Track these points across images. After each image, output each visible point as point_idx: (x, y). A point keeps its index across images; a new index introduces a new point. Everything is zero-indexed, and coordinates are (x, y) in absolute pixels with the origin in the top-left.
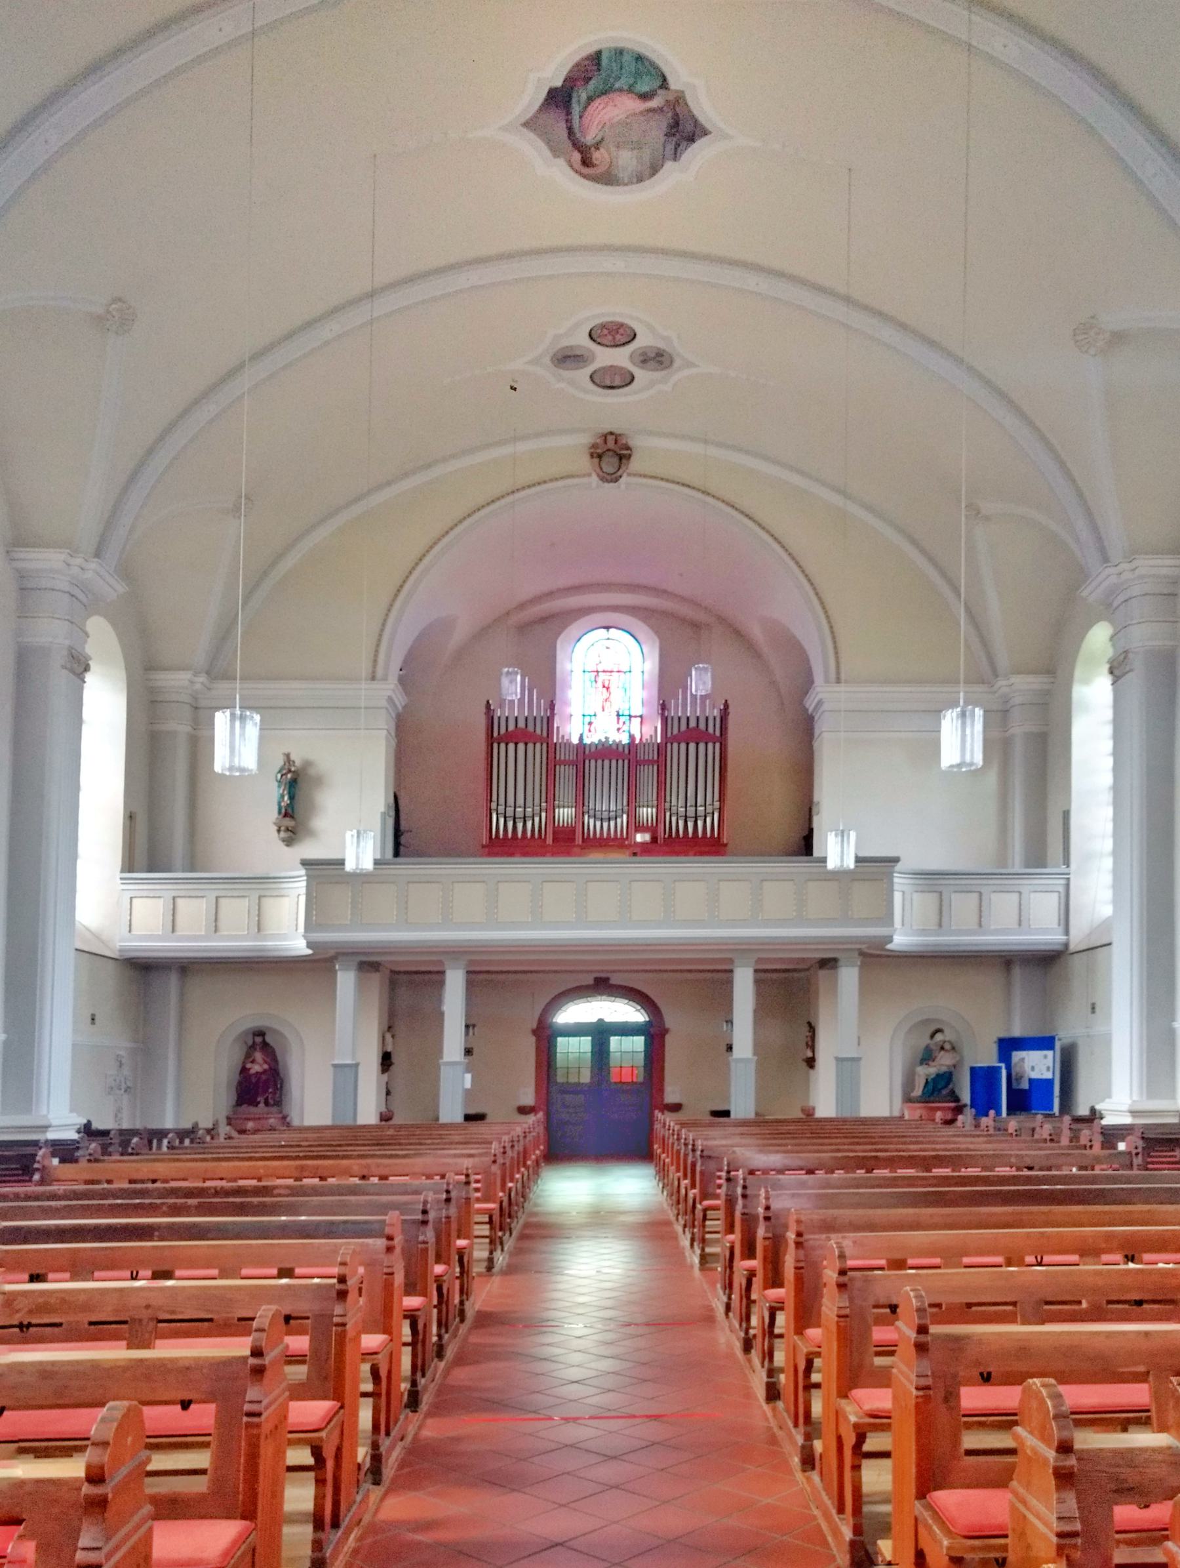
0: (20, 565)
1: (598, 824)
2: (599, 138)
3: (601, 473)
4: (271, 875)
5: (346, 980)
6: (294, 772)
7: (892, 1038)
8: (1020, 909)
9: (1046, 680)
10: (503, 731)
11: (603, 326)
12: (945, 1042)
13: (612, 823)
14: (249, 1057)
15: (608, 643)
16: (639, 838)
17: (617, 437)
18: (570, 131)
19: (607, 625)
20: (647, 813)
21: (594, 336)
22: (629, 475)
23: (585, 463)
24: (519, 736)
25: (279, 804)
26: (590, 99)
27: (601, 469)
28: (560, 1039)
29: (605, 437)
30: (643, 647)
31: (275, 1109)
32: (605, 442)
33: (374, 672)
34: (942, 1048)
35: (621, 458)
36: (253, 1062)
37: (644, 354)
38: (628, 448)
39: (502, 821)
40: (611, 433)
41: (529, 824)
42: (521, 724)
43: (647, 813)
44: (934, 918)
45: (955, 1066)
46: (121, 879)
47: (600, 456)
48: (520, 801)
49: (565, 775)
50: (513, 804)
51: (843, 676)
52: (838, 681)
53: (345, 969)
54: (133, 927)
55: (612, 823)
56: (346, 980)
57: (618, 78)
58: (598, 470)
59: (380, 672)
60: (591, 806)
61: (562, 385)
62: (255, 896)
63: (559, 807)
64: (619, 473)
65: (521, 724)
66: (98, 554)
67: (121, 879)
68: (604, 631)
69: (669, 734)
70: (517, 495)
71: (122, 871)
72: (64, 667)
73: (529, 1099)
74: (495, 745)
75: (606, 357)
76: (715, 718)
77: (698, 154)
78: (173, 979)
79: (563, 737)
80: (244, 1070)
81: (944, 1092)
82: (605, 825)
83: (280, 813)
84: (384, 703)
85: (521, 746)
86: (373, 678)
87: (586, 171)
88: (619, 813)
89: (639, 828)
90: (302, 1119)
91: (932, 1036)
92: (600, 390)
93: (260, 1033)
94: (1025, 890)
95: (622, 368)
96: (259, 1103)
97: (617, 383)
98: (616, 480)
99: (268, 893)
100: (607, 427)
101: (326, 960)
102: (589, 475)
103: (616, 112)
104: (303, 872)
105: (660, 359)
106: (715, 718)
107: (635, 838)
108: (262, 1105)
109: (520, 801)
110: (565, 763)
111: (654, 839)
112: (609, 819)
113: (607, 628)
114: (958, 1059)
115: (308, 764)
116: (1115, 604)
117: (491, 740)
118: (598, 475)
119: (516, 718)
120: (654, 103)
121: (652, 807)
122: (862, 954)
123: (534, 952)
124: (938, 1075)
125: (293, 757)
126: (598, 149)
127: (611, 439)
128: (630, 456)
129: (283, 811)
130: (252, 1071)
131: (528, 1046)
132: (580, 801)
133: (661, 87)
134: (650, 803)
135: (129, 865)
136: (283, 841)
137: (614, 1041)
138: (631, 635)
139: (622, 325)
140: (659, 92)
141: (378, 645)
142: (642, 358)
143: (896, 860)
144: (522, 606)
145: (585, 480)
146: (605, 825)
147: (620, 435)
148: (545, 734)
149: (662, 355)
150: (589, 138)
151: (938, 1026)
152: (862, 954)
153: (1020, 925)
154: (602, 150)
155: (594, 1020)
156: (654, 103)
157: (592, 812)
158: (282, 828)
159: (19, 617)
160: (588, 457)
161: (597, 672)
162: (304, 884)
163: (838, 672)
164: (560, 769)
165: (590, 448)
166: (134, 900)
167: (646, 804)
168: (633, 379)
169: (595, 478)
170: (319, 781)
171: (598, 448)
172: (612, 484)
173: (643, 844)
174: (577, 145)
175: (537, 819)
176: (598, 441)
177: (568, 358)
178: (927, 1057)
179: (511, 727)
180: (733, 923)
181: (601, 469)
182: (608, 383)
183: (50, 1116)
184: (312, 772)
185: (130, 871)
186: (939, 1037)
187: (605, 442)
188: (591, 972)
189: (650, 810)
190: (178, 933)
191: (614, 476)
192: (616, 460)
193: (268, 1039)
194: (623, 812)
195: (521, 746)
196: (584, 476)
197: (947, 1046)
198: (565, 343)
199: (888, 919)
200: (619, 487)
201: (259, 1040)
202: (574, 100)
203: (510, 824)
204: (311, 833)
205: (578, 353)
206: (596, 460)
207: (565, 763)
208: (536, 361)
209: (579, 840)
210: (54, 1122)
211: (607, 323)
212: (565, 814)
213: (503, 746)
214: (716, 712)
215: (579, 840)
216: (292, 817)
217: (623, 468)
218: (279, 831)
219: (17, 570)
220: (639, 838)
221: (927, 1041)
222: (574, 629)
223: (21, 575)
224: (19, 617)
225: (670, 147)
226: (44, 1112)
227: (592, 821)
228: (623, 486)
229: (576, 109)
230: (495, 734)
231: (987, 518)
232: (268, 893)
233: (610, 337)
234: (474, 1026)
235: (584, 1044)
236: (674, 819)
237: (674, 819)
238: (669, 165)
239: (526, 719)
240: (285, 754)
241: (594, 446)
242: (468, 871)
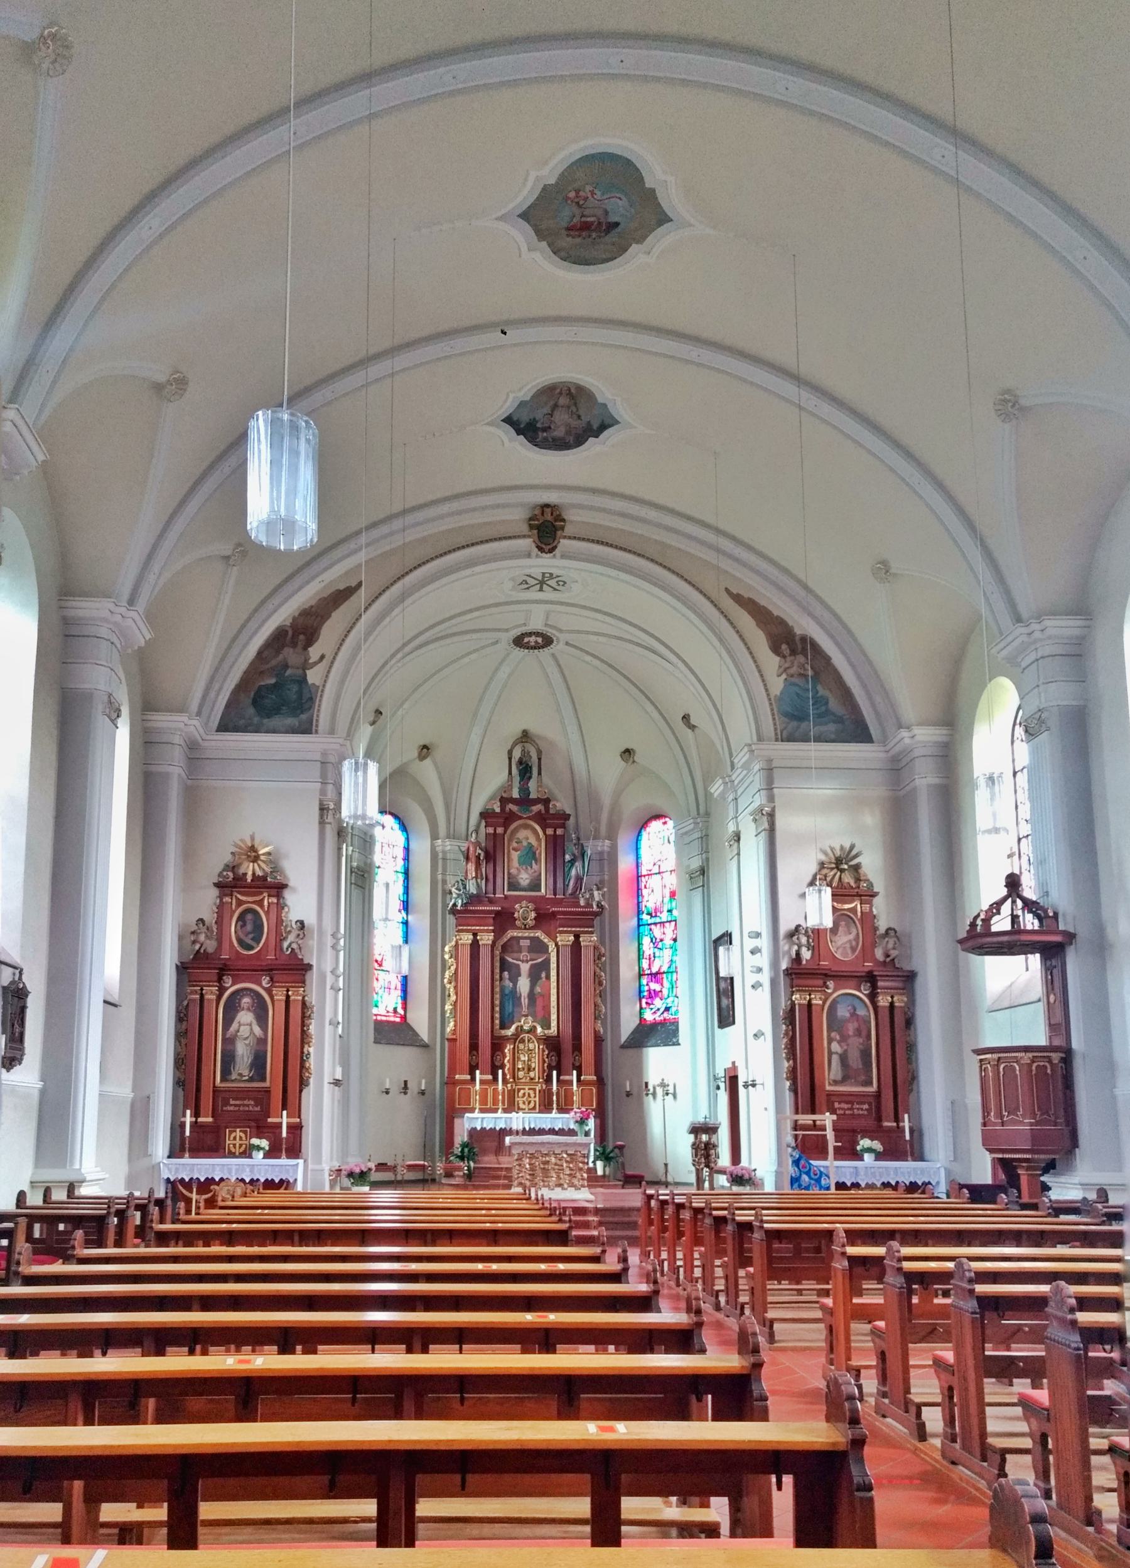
0: (149, 724)
9: (945, 732)
32: (543, 514)
38: (564, 520)
116: (1024, 665)
127: (548, 510)
165: (530, 519)
183: (83, 1171)
187: (543, 514)
188: (324, 686)
210: (88, 1179)
226: (77, 1167)
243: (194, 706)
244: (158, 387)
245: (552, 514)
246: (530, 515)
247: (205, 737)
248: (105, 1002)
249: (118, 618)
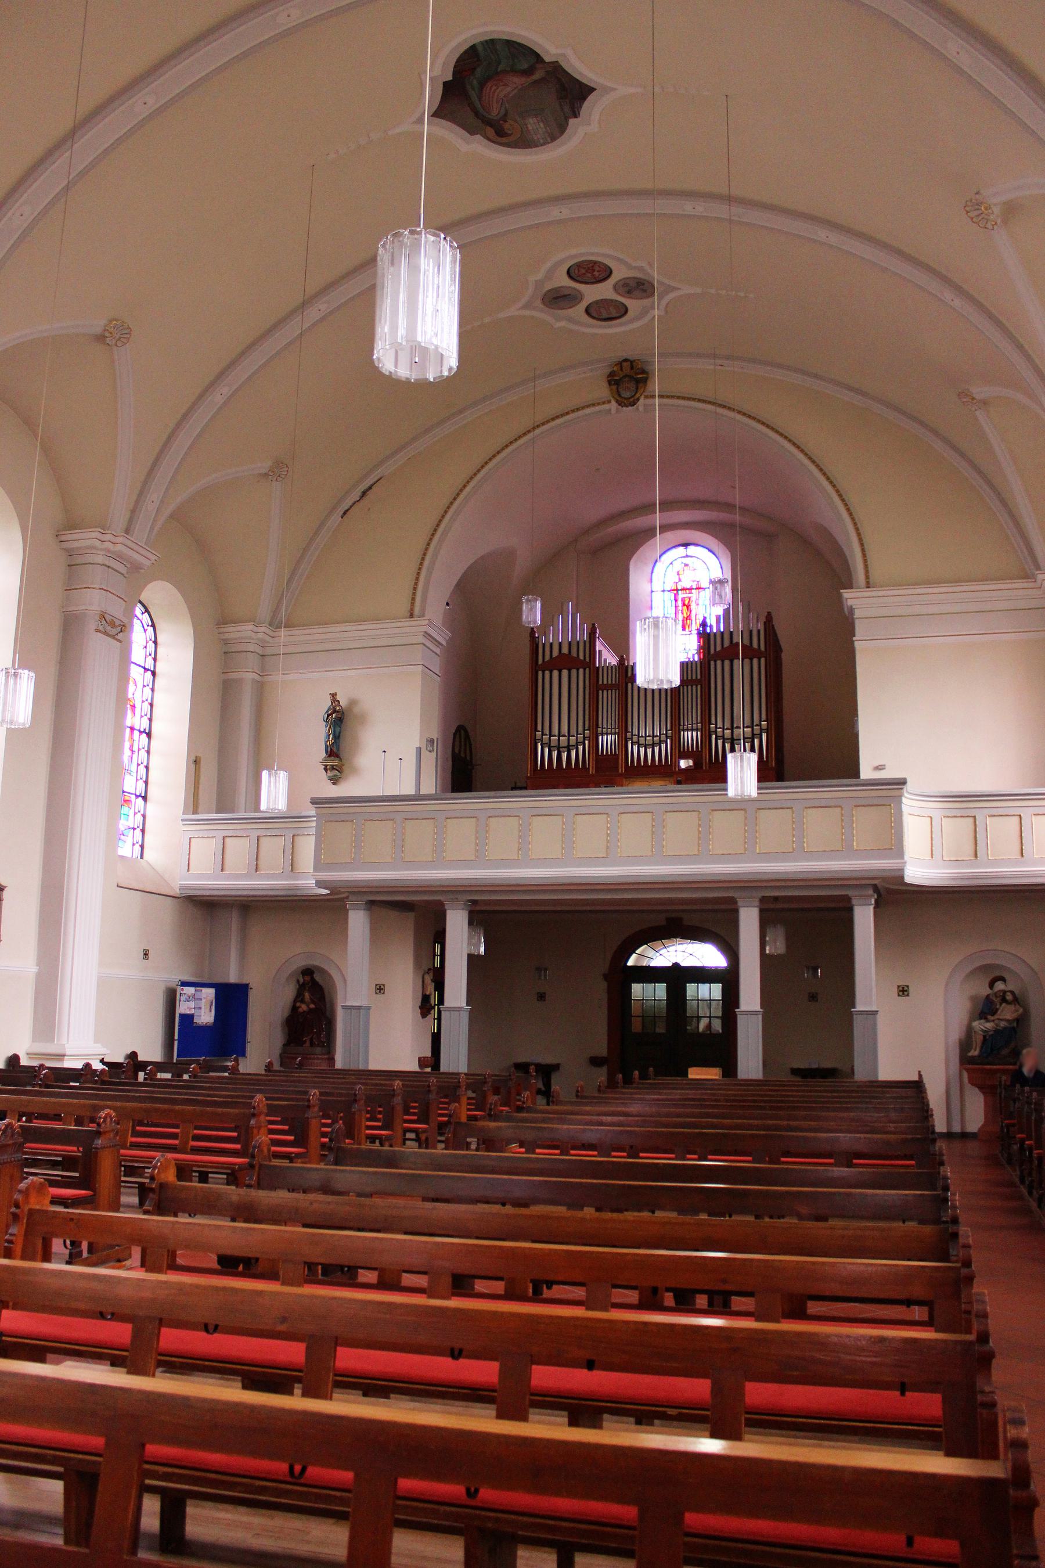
0: (65, 545)
1: (642, 750)
2: (503, 112)
3: (619, 399)
4: (303, 814)
5: (358, 921)
6: (338, 712)
7: (947, 985)
8: (144, 891)
10: (547, 658)
11: (579, 265)
12: (1005, 992)
13: (657, 749)
14: (299, 997)
15: (687, 561)
16: (683, 764)
17: (632, 363)
18: (477, 114)
19: (685, 542)
20: (690, 737)
21: (573, 275)
22: (646, 397)
23: (603, 391)
24: (566, 661)
25: (326, 742)
26: (482, 85)
27: (620, 396)
28: (634, 985)
29: (620, 364)
30: (721, 560)
31: (318, 1050)
32: (621, 369)
33: (412, 610)
34: (1004, 1000)
35: (638, 382)
36: (303, 1001)
37: (625, 285)
38: (643, 372)
39: (547, 750)
40: (626, 360)
41: (573, 753)
42: (565, 650)
43: (690, 737)
44: (969, 848)
45: (1017, 1020)
46: (183, 820)
47: (617, 383)
48: (565, 729)
49: (608, 700)
50: (557, 734)
51: (876, 575)
52: (868, 586)
53: (356, 908)
54: (191, 867)
55: (657, 749)
56: (358, 921)
57: (499, 63)
58: (616, 396)
59: (417, 610)
60: (635, 732)
61: (563, 324)
62: (289, 835)
63: (684, 731)
64: (638, 395)
65: (565, 650)
66: (127, 531)
67: (183, 820)
68: (682, 549)
69: (712, 651)
70: (537, 431)
71: (184, 813)
72: (97, 631)
73: (602, 1050)
74: (540, 673)
75: (593, 293)
76: (759, 631)
77: (593, 108)
78: (234, 920)
79: (605, 660)
80: (294, 1009)
81: (1005, 1052)
82: (649, 751)
83: (327, 752)
84: (421, 639)
85: (565, 672)
86: (411, 616)
87: (504, 140)
88: (663, 738)
89: (684, 755)
90: (367, 1062)
91: (991, 985)
92: (599, 323)
93: (308, 972)
94: (1026, 814)
95: (612, 301)
96: (305, 1042)
97: (614, 314)
98: (633, 404)
99: (301, 832)
100: (625, 355)
101: (342, 900)
102: (609, 402)
103: (509, 89)
104: (313, 813)
105: (641, 287)
106: (759, 631)
107: (679, 766)
108: (308, 1044)
109: (565, 729)
110: (608, 687)
111: (697, 764)
112: (653, 746)
113: (686, 545)
114: (1021, 1010)
115: (353, 703)
117: (535, 668)
118: (617, 401)
119: (560, 644)
120: (537, 76)
121: (697, 730)
122: (876, 888)
123: (545, 891)
124: (997, 1032)
125: (338, 698)
126: (505, 121)
128: (645, 381)
129: (329, 750)
130: (300, 1010)
131: (599, 991)
132: (623, 731)
133: (537, 62)
134: (605, 730)
135: (194, 805)
136: (331, 780)
137: (691, 988)
138: (710, 550)
139: (595, 263)
140: (538, 66)
141: (416, 584)
142: (626, 289)
143: (903, 782)
144: (587, 532)
145: (606, 406)
146: (649, 751)
147: (634, 361)
148: (587, 659)
149: (643, 284)
150: (495, 112)
151: (997, 973)
152: (876, 888)
153: (1022, 855)
154: (510, 122)
155: (670, 964)
156: (537, 76)
157: (635, 739)
158: (328, 767)
159: (66, 590)
160: (606, 384)
161: (677, 590)
162: (314, 824)
163: (867, 577)
164: (604, 695)
165: (608, 376)
166: (192, 839)
167: (609, 730)
168: (626, 311)
169: (614, 403)
170: (362, 719)
171: (615, 376)
172: (630, 408)
173: (687, 769)
174: (489, 123)
175: (581, 748)
176: (615, 369)
177: (557, 299)
178: (986, 1009)
179: (555, 653)
180: (678, 858)
181: (620, 396)
182: (605, 315)
184: (356, 710)
185: (195, 812)
186: (1000, 986)
187: (621, 369)
189: (694, 733)
190: (227, 872)
191: (631, 400)
192: (632, 385)
193: (317, 977)
194: (667, 737)
195: (565, 672)
196: (604, 403)
197: (1009, 997)
198: (548, 286)
199: (896, 848)
200: (638, 409)
201: (307, 978)
202: (468, 87)
203: (555, 754)
204: (355, 771)
205: (566, 293)
206: (614, 387)
207: (608, 687)
208: (527, 306)
209: (622, 769)
210: (67, 1053)
211: (583, 262)
212: (607, 741)
213: (547, 673)
214: (761, 626)
215: (622, 769)
216: (337, 756)
217: (640, 391)
218: (326, 770)
219: (66, 550)
220: (683, 764)
221: (988, 991)
222: (647, 551)
223: (70, 553)
224: (66, 590)
225: (567, 109)
227: (635, 748)
228: (641, 409)
229: (474, 95)
230: (540, 662)
231: (985, 403)
232: (301, 832)
233: (589, 275)
234: (546, 970)
235: (660, 991)
236: (720, 742)
237: (720, 742)
238: (572, 121)
239: (570, 643)
240: (331, 694)
241: (611, 374)
242: (544, 804)
243: (119, 516)
244: (101, 338)
245: (632, 368)
246: (608, 371)
247: (272, 634)
248: (118, 886)
249: (107, 545)
